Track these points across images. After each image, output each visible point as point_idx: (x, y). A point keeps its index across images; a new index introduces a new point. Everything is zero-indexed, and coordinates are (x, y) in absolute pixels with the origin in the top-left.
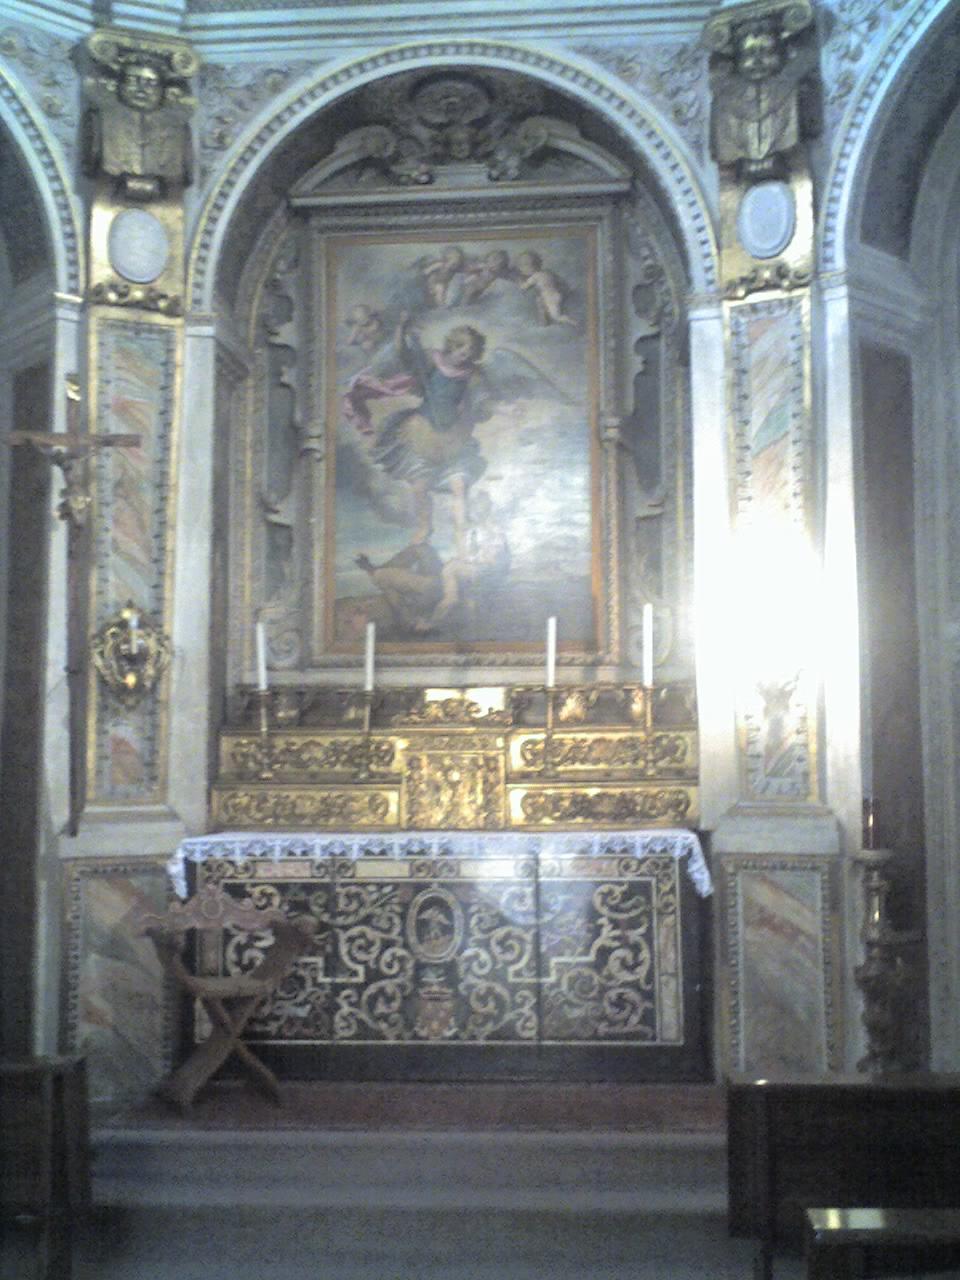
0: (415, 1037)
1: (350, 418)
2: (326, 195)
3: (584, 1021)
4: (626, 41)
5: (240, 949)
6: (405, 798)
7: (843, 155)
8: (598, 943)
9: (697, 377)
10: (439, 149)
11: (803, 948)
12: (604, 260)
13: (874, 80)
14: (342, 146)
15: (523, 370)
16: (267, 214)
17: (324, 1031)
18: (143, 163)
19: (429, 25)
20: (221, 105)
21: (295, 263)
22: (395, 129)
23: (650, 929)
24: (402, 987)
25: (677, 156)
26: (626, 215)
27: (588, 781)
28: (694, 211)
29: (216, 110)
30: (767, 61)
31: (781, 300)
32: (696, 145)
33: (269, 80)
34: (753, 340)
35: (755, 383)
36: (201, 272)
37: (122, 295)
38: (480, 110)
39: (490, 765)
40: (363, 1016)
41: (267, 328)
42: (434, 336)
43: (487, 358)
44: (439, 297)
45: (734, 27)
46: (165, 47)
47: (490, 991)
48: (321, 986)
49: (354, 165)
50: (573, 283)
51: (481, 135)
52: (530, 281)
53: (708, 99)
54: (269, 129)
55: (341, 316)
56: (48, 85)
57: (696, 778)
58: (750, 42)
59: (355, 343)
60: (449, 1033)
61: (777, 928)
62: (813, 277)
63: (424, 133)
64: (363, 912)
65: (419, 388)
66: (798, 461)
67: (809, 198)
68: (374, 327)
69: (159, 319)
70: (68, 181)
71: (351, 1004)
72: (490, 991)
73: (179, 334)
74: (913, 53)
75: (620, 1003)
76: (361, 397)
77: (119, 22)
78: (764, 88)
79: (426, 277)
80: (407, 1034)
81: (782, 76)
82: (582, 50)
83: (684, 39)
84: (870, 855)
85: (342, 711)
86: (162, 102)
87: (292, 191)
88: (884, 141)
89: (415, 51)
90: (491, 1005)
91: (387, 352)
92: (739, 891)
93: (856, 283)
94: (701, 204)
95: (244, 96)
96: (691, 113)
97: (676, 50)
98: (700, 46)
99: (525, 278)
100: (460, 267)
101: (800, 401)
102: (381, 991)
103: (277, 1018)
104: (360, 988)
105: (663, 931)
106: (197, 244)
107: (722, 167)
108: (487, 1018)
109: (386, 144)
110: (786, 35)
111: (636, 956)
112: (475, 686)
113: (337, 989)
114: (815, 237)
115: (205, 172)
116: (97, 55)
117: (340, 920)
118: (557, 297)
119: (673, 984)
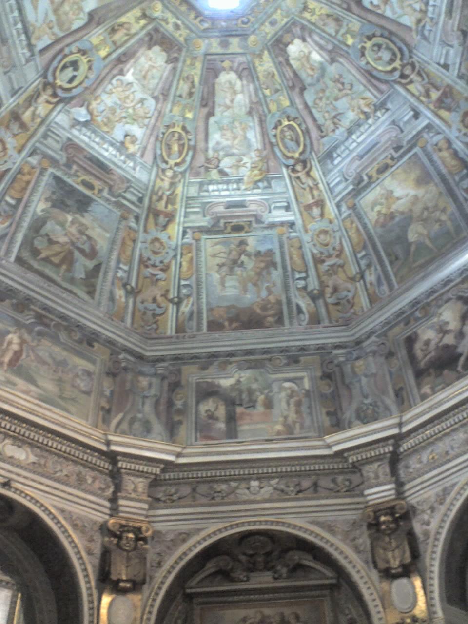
2: (202, 587)
4: (331, 518)
7: (432, 565)
10: (251, 566)
13: (438, 533)
18: (127, 575)
25: (359, 567)
28: (370, 591)
29: (158, 550)
32: (367, 562)
33: (181, 537)
38: (268, 549)
46: (139, 524)
53: (368, 542)
54: (181, 558)
56: (89, 541)
58: (383, 519)
63: (243, 558)
70: (93, 583)
74: (453, 522)
78: (393, 537)
82: (312, 523)
83: (354, 517)
86: (135, 548)
87: (187, 586)
89: (243, 524)
94: (372, 588)
97: (352, 521)
98: (361, 520)
107: (380, 571)
110: (397, 515)
115: (151, 578)
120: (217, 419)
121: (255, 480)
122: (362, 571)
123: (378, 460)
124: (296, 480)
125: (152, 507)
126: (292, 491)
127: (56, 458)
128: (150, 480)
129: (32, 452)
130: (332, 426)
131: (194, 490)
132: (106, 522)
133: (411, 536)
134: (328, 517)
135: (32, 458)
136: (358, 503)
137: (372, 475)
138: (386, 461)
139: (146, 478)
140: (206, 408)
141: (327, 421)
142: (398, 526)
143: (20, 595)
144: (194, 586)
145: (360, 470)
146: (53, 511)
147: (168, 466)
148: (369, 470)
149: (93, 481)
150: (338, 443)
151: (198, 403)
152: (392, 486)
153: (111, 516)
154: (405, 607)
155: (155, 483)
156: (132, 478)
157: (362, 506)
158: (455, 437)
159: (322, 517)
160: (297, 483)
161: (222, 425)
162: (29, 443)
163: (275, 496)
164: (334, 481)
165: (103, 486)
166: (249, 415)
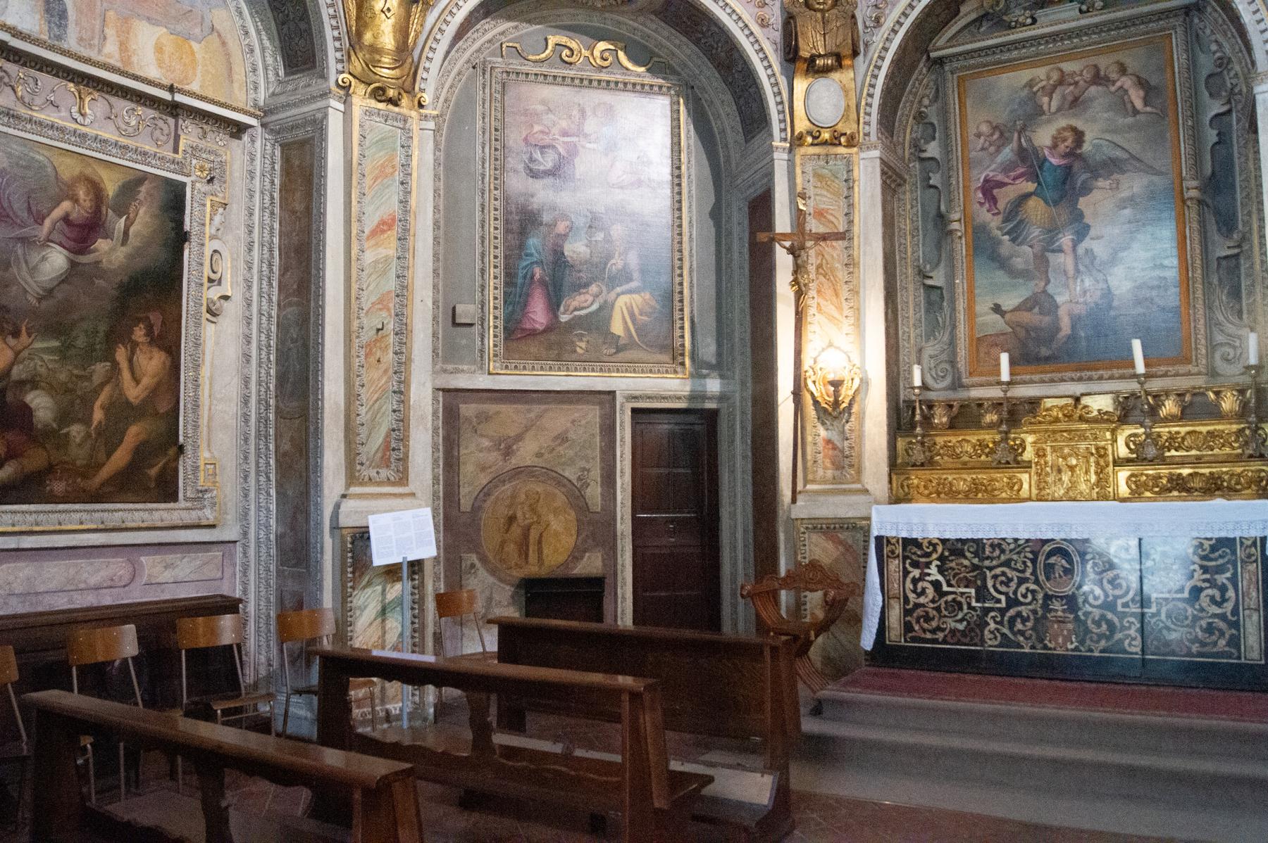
0: (1045, 647)
1: (981, 204)
5: (915, 581)
6: (1035, 478)
12: (1180, 58)
14: (964, 9)
15: (1118, 153)
16: (913, 67)
17: (977, 640)
24: (1035, 612)
26: (1196, 20)
27: (1182, 463)
37: (815, 138)
39: (1101, 453)
40: (1006, 631)
43: (1087, 147)
44: (1045, 107)
47: (1103, 617)
48: (974, 609)
52: (1118, 84)
55: (972, 130)
59: (983, 149)
60: (1070, 646)
64: (1003, 558)
70: (777, 67)
71: (996, 623)
72: (1103, 617)
73: (855, 158)
79: (1035, 93)
90: (1104, 627)
91: (1007, 153)
99: (1114, 82)
100: (1061, 82)
103: (943, 630)
104: (1003, 612)
105: (1246, 576)
106: (865, 95)
111: (1223, 596)
113: (986, 611)
115: (867, 45)
117: (987, 563)
118: (1142, 93)
119: (1255, 617)
143: (681, 101)
144: (942, 46)
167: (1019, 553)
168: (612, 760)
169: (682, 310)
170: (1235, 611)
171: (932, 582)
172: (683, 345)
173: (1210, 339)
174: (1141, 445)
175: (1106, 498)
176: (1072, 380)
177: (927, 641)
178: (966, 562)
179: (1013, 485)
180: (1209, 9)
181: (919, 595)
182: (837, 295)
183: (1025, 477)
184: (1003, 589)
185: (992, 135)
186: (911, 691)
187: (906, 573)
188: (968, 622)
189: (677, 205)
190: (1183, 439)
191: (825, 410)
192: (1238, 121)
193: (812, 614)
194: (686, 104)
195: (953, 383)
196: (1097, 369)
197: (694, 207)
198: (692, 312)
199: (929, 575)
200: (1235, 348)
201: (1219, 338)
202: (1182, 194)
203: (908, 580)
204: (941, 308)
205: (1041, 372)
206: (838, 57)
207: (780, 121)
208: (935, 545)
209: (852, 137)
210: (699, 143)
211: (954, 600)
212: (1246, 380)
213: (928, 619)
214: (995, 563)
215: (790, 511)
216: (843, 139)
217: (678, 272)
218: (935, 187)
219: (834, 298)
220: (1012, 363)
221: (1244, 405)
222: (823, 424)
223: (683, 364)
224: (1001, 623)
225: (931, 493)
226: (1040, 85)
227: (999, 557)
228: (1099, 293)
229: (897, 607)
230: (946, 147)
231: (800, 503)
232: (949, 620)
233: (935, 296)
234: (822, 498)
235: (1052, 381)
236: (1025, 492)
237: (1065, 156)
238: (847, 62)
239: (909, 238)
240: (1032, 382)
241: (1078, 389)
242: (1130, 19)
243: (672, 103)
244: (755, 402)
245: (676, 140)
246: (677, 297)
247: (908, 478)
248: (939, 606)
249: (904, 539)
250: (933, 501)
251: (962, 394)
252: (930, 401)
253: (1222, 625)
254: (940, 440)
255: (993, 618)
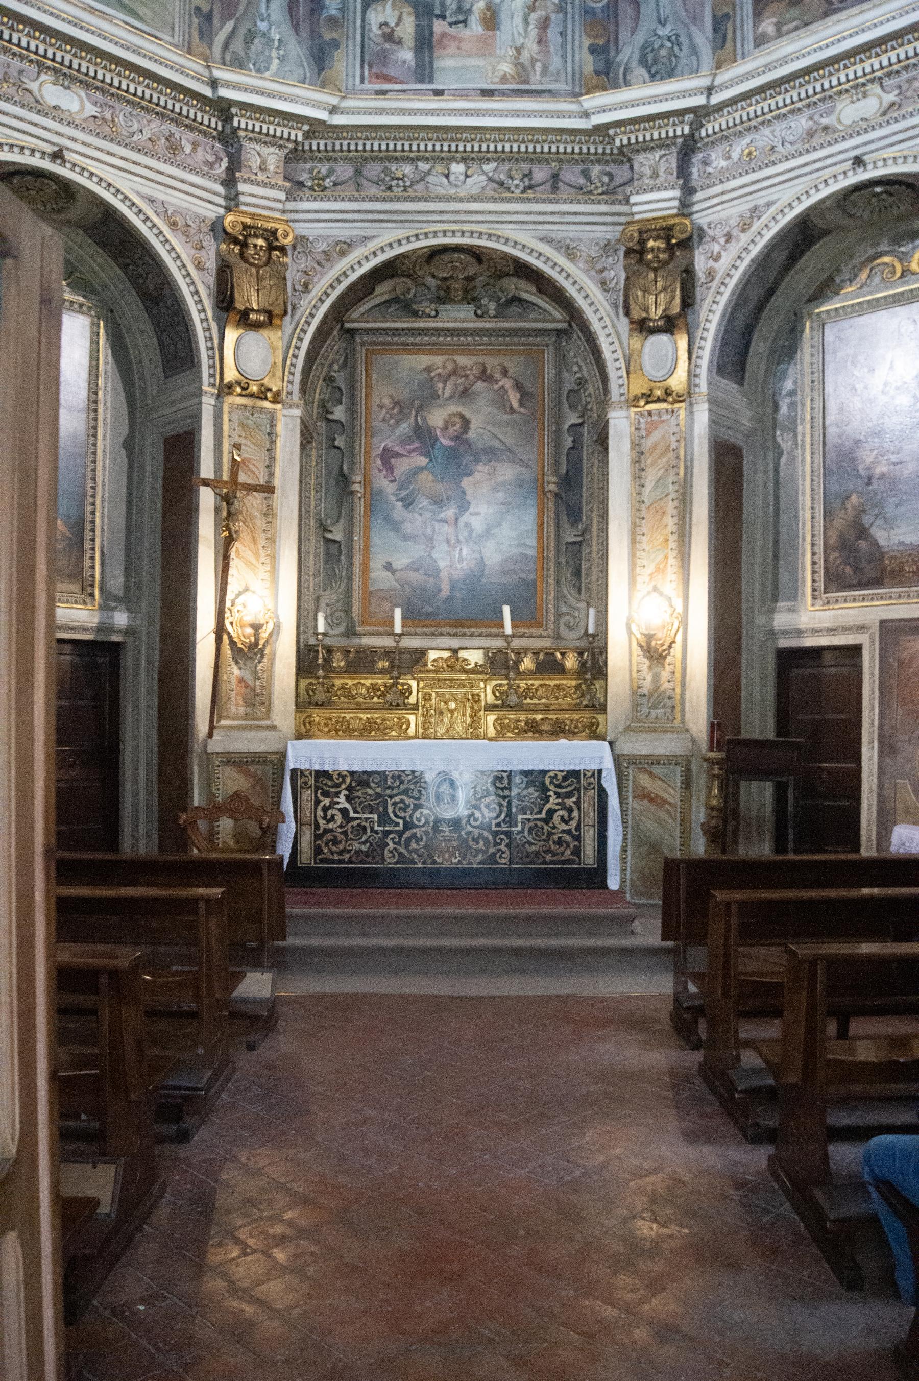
0: (434, 862)
1: (380, 471)
3: (537, 854)
4: (572, 235)
5: (325, 809)
6: (421, 719)
8: (548, 806)
9: (612, 454)
11: (668, 811)
12: (549, 372)
14: (378, 290)
15: (496, 444)
16: (329, 334)
17: (377, 859)
19: (444, 217)
20: (305, 263)
21: (344, 366)
22: (415, 280)
23: (579, 799)
24: (426, 833)
25: (602, 312)
26: (564, 343)
27: (536, 711)
28: (612, 348)
30: (662, 256)
31: (667, 410)
32: (615, 305)
34: (649, 434)
35: (649, 462)
36: (292, 374)
37: (243, 389)
38: (471, 271)
39: (476, 699)
40: (402, 850)
41: (325, 409)
42: (436, 418)
43: (471, 434)
44: (440, 392)
45: (641, 233)
46: (273, 225)
47: (481, 836)
48: (376, 832)
49: (387, 302)
50: (528, 385)
51: (471, 285)
52: (500, 384)
53: (623, 276)
55: (375, 401)
57: (605, 710)
58: (651, 243)
59: (384, 420)
60: (454, 861)
61: (653, 800)
62: (686, 397)
63: (431, 282)
64: (402, 787)
65: (428, 455)
66: (675, 512)
67: (686, 346)
68: (396, 410)
69: (267, 404)
71: (394, 843)
72: (481, 836)
73: (279, 415)
75: (560, 842)
76: (388, 456)
77: (243, 208)
78: (660, 273)
79: (432, 378)
80: (430, 861)
81: (671, 266)
84: (714, 755)
85: (373, 663)
87: (345, 318)
88: (732, 313)
90: (482, 843)
91: (405, 427)
92: (631, 777)
93: (713, 401)
94: (617, 343)
95: (321, 258)
96: (612, 285)
98: (619, 241)
99: (497, 382)
100: (454, 373)
101: (678, 474)
102: (414, 835)
103: (349, 851)
104: (400, 834)
105: (587, 799)
106: (290, 355)
108: (479, 851)
109: (409, 290)
110: (674, 241)
111: (570, 816)
112: (466, 649)
113: (387, 833)
114: (689, 370)
115: (294, 307)
116: (229, 230)
117: (388, 792)
118: (518, 396)
119: (591, 832)
120: (399, 43)
121: (458, 163)
122: (606, 319)
123: (660, 147)
124: (526, 167)
125: (290, 197)
126: (517, 186)
127: (128, 109)
128: (287, 151)
129: (89, 98)
130: (597, 73)
131: (359, 172)
132: (221, 219)
133: (689, 273)
134: (571, 232)
135: (91, 110)
136: (620, 214)
137: (647, 171)
138: (674, 150)
139: (280, 146)
140: (381, 19)
141: (588, 63)
142: (672, 256)
143: (102, 324)
144: (356, 319)
145: (630, 160)
146: (137, 200)
147: (315, 128)
148: (644, 162)
149: (194, 149)
150: (603, 110)
151: (365, 7)
152: (677, 193)
153: (228, 209)
154: (659, 375)
155: (295, 155)
156: (258, 147)
157: (623, 219)
158: (793, 124)
159: (557, 232)
160: (526, 172)
161: (407, 55)
162: (81, 82)
163: (489, 192)
164: (586, 174)
165: (211, 159)
166: (454, 38)
167: (415, 783)
168: (38, 993)
169: (93, 540)
170: (578, 828)
171: (340, 810)
172: (93, 576)
173: (557, 608)
174: (506, 693)
175: (477, 737)
176: (450, 635)
177: (334, 862)
178: (370, 792)
179: (402, 725)
180: (575, 337)
181: (328, 822)
182: (254, 541)
183: (412, 718)
184: (401, 814)
185: (393, 409)
186: (319, 904)
187: (317, 802)
188: (371, 845)
189: (92, 432)
190: (537, 690)
191: (240, 651)
192: (589, 432)
193: (224, 842)
194: (106, 326)
195: (347, 629)
196: (469, 627)
197: (108, 435)
198: (102, 543)
199: (338, 803)
200: (574, 617)
201: (564, 609)
202: (543, 488)
203: (320, 808)
204: (339, 560)
205: (423, 626)
206: (270, 314)
207: (210, 367)
208: (344, 777)
209: (278, 394)
210: (116, 370)
211: (359, 825)
212: (584, 643)
213: (336, 842)
214: (395, 792)
215: (205, 745)
216: (269, 395)
217: (91, 500)
218: (338, 448)
219: (252, 545)
220: (404, 618)
221: (583, 664)
222: (237, 663)
223: (92, 595)
224: (399, 843)
225: (330, 731)
226: (437, 372)
227: (399, 787)
228: (474, 562)
229: (308, 833)
230: (352, 410)
231: (216, 737)
232: (355, 843)
233: (333, 549)
234: (236, 734)
235: (433, 634)
236: (411, 731)
237: (455, 438)
238: (276, 321)
239: (313, 493)
240: (416, 634)
241: (455, 643)
242: (514, 330)
243: (92, 324)
244: (164, 638)
245: (94, 363)
246: (88, 526)
247: (310, 716)
248: (346, 832)
249: (317, 772)
250: (332, 738)
251: (355, 641)
252: (330, 646)
253: (567, 838)
254: (338, 682)
255: (392, 839)
